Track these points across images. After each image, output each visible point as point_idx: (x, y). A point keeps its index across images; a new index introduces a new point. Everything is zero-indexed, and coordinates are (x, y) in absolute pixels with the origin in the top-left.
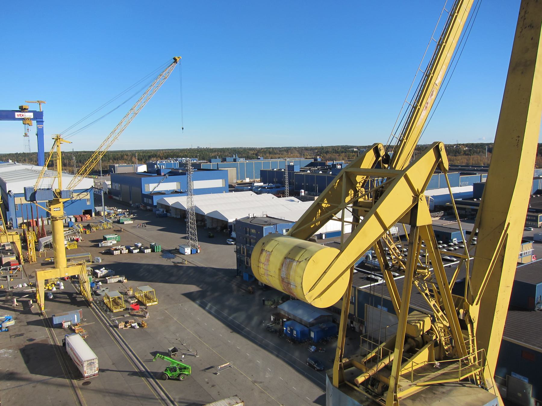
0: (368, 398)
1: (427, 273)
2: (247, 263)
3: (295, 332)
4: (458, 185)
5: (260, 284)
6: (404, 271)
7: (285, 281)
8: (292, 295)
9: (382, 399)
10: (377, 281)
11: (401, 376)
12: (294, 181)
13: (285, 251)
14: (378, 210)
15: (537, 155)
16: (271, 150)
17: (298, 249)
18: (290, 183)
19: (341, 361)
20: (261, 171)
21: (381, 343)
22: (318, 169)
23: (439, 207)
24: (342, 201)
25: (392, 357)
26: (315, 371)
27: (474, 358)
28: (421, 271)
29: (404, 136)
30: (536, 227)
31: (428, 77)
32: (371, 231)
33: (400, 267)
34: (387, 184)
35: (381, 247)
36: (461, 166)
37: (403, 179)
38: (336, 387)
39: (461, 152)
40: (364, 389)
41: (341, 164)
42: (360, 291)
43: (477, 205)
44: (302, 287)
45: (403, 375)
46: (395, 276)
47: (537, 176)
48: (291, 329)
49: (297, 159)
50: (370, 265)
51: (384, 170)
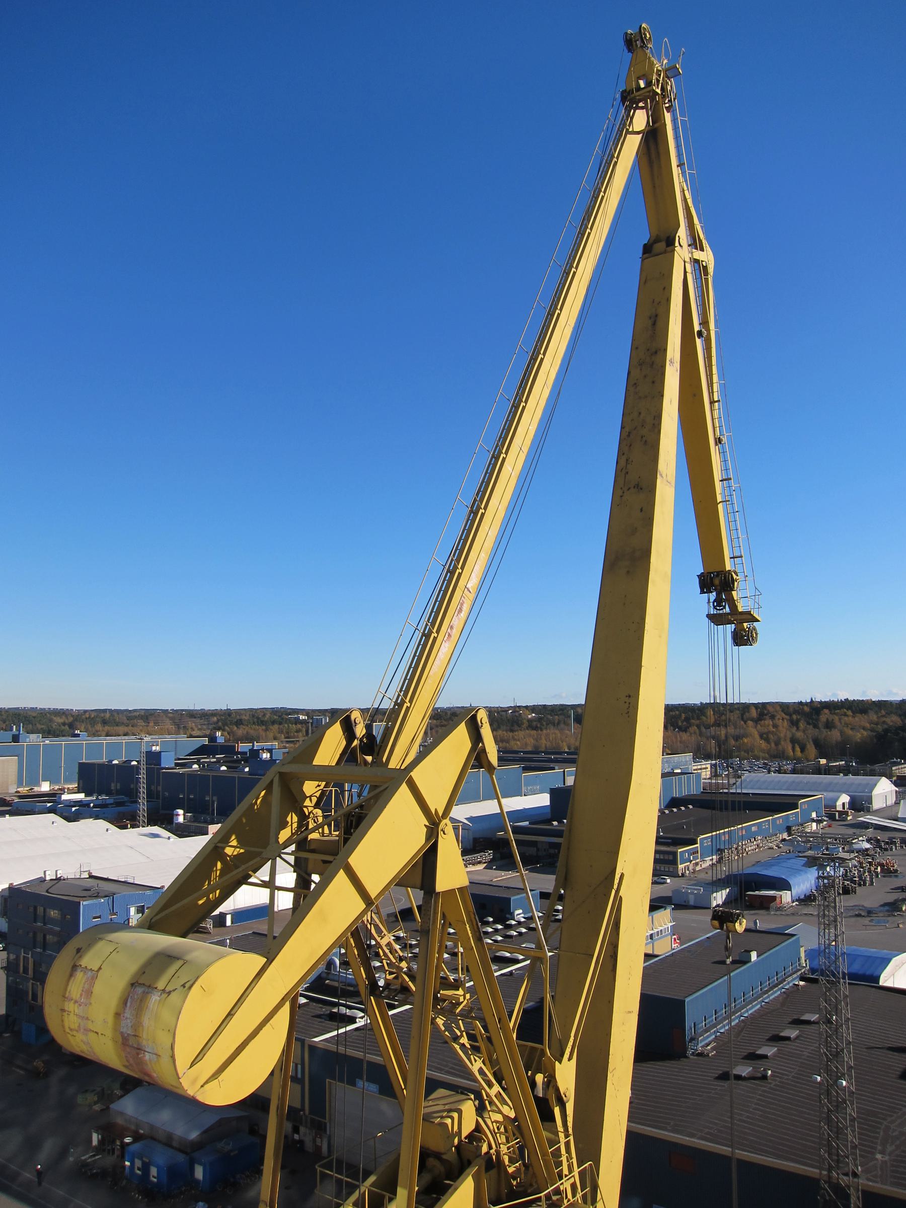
3: (154, 1171)
4: (518, 793)
7: (130, 1043)
8: (147, 1078)
10: (352, 1020)
12: (160, 788)
13: (133, 968)
14: (353, 860)
15: (665, 727)
16: (108, 715)
21: (367, 1175)
22: (218, 761)
23: (481, 841)
24: (272, 840)
27: (573, 1186)
29: (405, 695)
30: (674, 875)
31: (451, 574)
32: (338, 908)
34: (370, 799)
35: (359, 944)
36: (525, 753)
37: (404, 788)
41: (270, 749)
42: (313, 1048)
43: (558, 834)
44: (173, 1057)
46: (392, 1007)
48: (144, 1163)
49: (169, 738)
50: (336, 984)
51: (363, 768)
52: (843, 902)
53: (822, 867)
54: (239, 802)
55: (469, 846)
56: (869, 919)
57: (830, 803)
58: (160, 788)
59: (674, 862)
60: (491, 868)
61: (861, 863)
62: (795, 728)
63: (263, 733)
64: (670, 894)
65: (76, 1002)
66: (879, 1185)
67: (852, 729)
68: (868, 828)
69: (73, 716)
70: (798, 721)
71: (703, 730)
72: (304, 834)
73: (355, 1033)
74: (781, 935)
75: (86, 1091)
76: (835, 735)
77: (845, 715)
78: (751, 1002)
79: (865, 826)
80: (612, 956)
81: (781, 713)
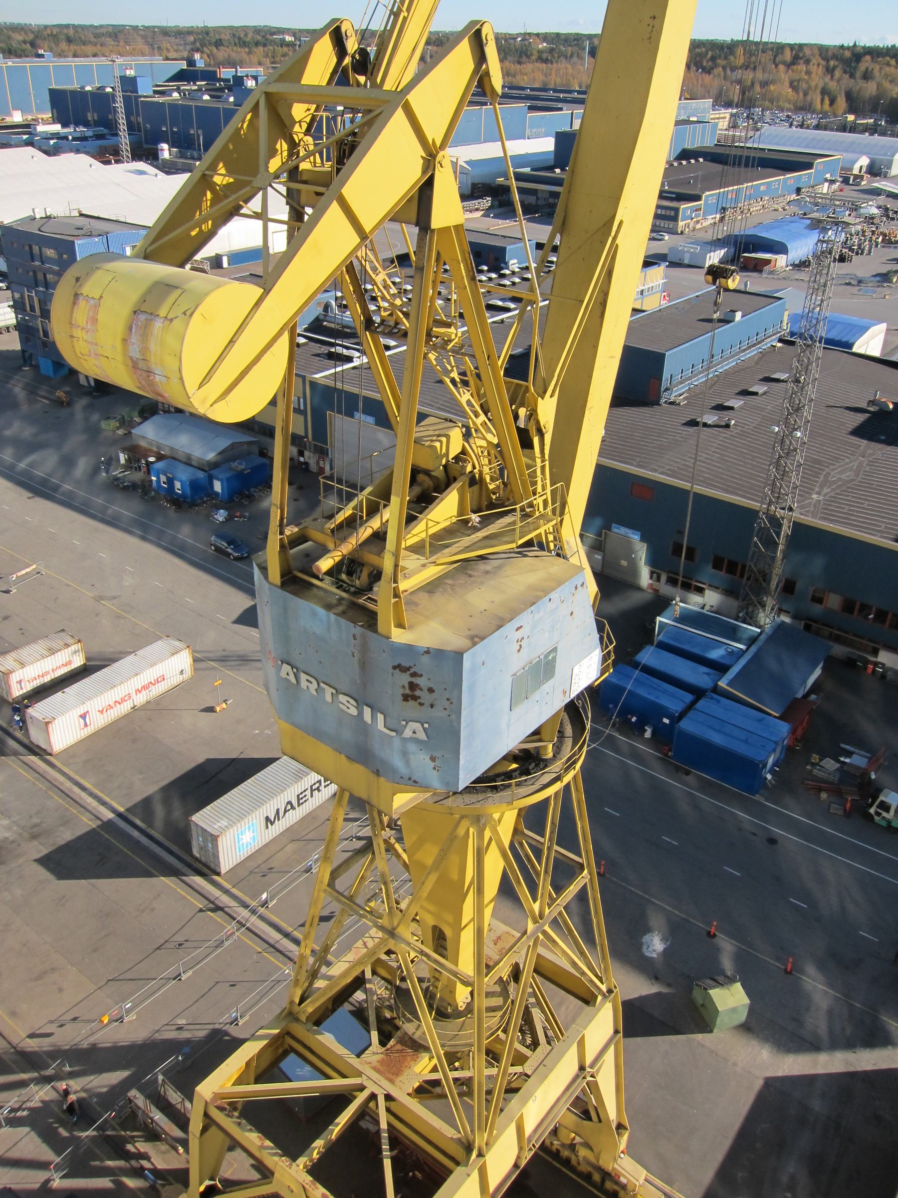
0: (341, 599)
1: (456, 333)
2: (46, 334)
3: (178, 485)
4: (522, 137)
5: (82, 381)
6: (405, 334)
8: (160, 399)
9: (369, 598)
10: (349, 359)
11: (406, 549)
12: (140, 120)
13: (134, 297)
14: (347, 191)
15: (688, 66)
17: (164, 288)
18: (131, 127)
19: (281, 533)
20: (52, 92)
21: (362, 489)
22: (200, 90)
24: (262, 169)
25: (387, 514)
26: (231, 558)
27: (545, 502)
28: (442, 330)
30: (673, 232)
33: (397, 324)
36: (532, 89)
37: (399, 115)
38: (276, 586)
39: (532, 54)
40: (333, 583)
41: (255, 75)
42: (314, 384)
43: (559, 182)
44: (181, 379)
45: (410, 546)
46: (388, 348)
47: (685, 117)
48: (168, 478)
50: (332, 325)
51: (355, 89)
52: (837, 269)
53: (825, 230)
54: (226, 124)
55: (467, 191)
56: (858, 288)
57: (848, 166)
58: (140, 120)
59: (675, 219)
60: (489, 216)
61: (864, 232)
62: (829, 77)
63: (245, 57)
64: (665, 251)
65: (83, 329)
66: (810, 519)
67: (891, 82)
68: (879, 195)
69: (33, 32)
70: (834, 68)
71: (729, 72)
72: (295, 162)
73: (353, 371)
74: (771, 298)
75: (108, 418)
76: (870, 89)
77: (888, 64)
78: (728, 359)
79: (877, 192)
80: (601, 304)
81: (817, 57)
